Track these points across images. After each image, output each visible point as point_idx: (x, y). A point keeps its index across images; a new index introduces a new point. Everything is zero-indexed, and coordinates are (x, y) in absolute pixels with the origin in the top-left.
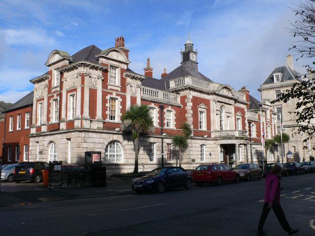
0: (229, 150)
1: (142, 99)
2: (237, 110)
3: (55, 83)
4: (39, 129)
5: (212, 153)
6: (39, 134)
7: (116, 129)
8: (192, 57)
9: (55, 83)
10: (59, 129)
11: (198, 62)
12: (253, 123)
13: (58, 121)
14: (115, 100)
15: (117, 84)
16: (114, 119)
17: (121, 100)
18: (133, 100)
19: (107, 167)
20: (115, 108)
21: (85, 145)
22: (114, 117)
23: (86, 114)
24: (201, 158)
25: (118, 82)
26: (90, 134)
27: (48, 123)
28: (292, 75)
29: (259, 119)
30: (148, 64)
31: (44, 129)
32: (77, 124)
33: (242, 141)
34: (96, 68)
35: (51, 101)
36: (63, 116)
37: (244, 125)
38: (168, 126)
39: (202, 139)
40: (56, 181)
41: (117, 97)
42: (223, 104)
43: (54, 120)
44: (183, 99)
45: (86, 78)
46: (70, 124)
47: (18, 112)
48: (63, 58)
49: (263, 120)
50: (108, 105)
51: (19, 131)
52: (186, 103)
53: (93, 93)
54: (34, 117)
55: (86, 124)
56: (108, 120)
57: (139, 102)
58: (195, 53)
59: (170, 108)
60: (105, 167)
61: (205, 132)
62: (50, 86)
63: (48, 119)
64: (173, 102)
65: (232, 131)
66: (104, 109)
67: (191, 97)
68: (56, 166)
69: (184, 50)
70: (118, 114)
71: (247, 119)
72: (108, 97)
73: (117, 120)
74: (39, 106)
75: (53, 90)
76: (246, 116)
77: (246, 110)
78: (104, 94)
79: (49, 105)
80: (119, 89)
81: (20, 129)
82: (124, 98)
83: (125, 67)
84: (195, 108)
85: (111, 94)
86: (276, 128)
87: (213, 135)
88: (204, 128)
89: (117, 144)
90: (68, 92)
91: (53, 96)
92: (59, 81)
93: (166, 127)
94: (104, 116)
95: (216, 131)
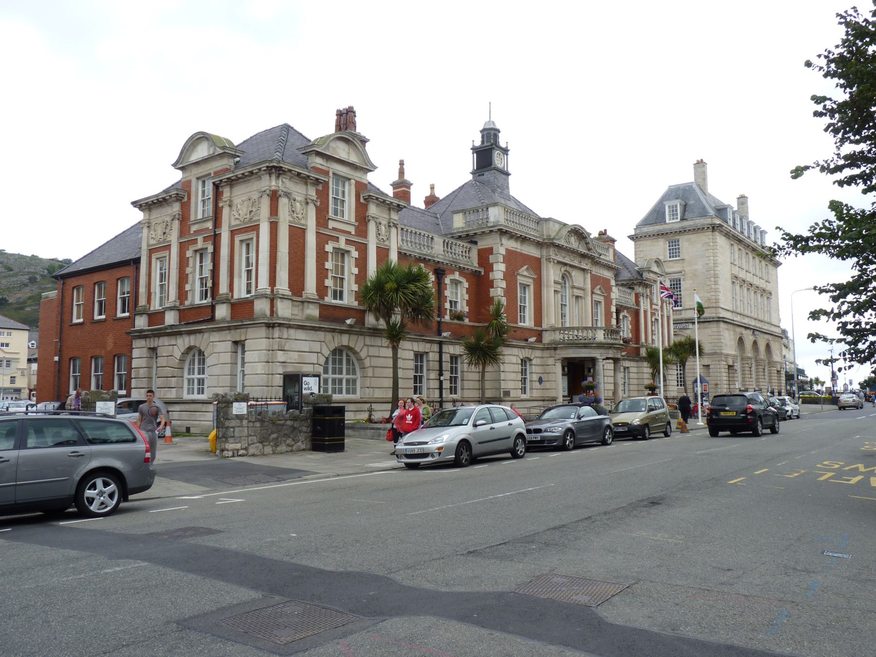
0: (578, 375)
1: (399, 253)
2: (596, 281)
3: (200, 209)
4: (156, 317)
5: (544, 377)
6: (158, 329)
7: (348, 322)
8: (498, 160)
9: (200, 209)
10: (212, 319)
11: (510, 171)
12: (625, 313)
13: (209, 299)
14: (456, 284)
15: (346, 218)
16: (341, 298)
17: (355, 254)
18: (383, 253)
19: (348, 407)
20: (343, 274)
21: (281, 356)
22: (341, 292)
23: (283, 285)
24: (415, 387)
25: (349, 212)
26: (292, 332)
27: (182, 303)
28: (707, 206)
29: (637, 303)
30: (402, 172)
31: (171, 318)
32: (261, 307)
33: (611, 351)
34: (304, 178)
35: (189, 254)
36: (223, 288)
37: (608, 314)
39: (523, 347)
40: (238, 439)
41: (348, 248)
42: (568, 268)
43: (196, 298)
44: (485, 256)
45: (283, 202)
46: (242, 310)
47: (97, 277)
48: (221, 151)
49: (644, 305)
50: (329, 265)
51: (100, 321)
52: (492, 264)
53: (297, 235)
54: (142, 290)
55: (284, 310)
56: (329, 300)
57: (394, 257)
58: (505, 151)
59: (457, 276)
60: (344, 407)
61: (530, 330)
62: (184, 219)
63: (182, 294)
64: (463, 262)
65: (586, 328)
66: (322, 273)
67: (503, 251)
68: (235, 404)
69: (478, 143)
70: (350, 287)
71: (614, 303)
72: (329, 248)
73: (349, 300)
74: (156, 266)
75: (194, 228)
76: (613, 296)
77: (613, 283)
78: (322, 240)
79: (183, 262)
80: (352, 230)
81: (81, 320)
82: (363, 249)
84: (510, 276)
86: (672, 322)
87: (547, 338)
88: (529, 322)
89: (347, 355)
90: (233, 233)
91: (195, 241)
92: (210, 207)
94: (322, 290)
95: (554, 330)
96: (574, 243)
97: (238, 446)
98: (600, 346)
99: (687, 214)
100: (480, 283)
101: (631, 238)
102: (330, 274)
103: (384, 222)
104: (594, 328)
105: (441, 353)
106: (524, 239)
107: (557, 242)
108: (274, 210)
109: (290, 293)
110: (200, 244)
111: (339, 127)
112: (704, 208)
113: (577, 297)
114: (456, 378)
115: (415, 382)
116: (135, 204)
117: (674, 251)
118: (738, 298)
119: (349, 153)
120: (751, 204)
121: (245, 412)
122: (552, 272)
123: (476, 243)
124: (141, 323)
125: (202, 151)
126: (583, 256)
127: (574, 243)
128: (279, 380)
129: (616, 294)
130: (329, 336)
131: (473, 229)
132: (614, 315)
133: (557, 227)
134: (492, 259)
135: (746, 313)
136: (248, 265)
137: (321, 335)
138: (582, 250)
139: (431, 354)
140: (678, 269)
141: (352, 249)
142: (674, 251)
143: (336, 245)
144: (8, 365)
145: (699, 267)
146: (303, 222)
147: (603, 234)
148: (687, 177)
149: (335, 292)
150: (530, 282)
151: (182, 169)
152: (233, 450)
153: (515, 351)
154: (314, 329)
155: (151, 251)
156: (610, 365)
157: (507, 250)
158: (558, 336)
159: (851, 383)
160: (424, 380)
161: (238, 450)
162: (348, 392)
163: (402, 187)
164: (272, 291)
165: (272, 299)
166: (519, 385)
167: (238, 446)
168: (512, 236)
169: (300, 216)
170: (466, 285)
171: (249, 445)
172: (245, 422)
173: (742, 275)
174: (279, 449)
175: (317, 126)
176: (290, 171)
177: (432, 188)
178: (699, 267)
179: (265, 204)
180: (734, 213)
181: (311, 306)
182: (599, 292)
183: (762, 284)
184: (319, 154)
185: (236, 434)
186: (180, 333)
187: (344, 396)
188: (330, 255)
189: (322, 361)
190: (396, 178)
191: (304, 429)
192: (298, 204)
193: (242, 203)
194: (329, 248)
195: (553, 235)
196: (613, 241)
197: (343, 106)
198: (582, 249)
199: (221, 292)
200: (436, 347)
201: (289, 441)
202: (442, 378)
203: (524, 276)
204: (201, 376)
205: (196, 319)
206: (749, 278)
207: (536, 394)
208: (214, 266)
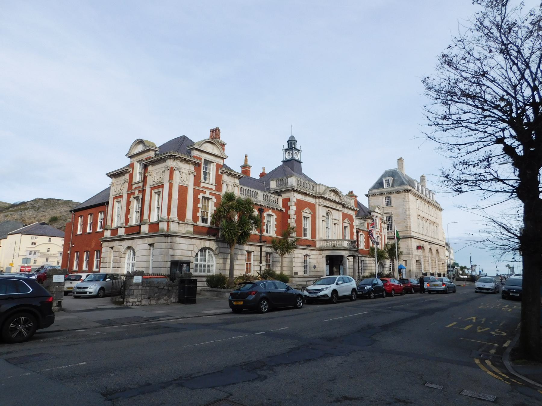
2: (345, 216)
3: (137, 177)
4: (114, 231)
6: (116, 238)
9: (137, 177)
10: (139, 233)
12: (361, 233)
15: (211, 182)
16: (206, 223)
19: (199, 279)
20: (208, 210)
23: (174, 215)
27: (126, 224)
30: (246, 161)
31: (121, 232)
32: (163, 226)
36: (145, 217)
37: (352, 234)
38: (267, 232)
40: (136, 296)
41: (210, 197)
42: (330, 209)
43: (134, 221)
44: (286, 202)
45: (176, 173)
50: (200, 205)
53: (183, 190)
54: (109, 217)
55: (174, 227)
56: (199, 223)
59: (270, 212)
63: (127, 220)
66: (196, 210)
71: (355, 227)
72: (200, 196)
75: (134, 186)
76: (354, 224)
77: (354, 217)
78: (196, 193)
79: (129, 203)
80: (213, 188)
83: (221, 162)
84: (298, 213)
85: (205, 192)
86: (386, 238)
87: (318, 245)
88: (309, 236)
89: (209, 252)
90: (152, 188)
91: (134, 193)
93: (265, 234)
94: (195, 218)
96: (333, 196)
97: (136, 300)
98: (345, 249)
99: (393, 184)
100: (283, 216)
101: (366, 195)
102: (200, 210)
103: (231, 184)
104: (343, 240)
105: (261, 251)
106: (306, 194)
107: (323, 196)
108: (171, 177)
109: (178, 219)
110: (136, 195)
111: (212, 137)
112: (403, 181)
113: (335, 224)
114: (269, 265)
115: (247, 266)
116: (108, 175)
117: (389, 203)
118: (428, 229)
119: (213, 149)
120: (405, 163)
121: (140, 281)
122: (321, 211)
123: (281, 196)
124: (108, 234)
125: (140, 148)
126: (338, 203)
127: (333, 196)
128: (169, 264)
129: (356, 222)
130: (198, 241)
131: (281, 188)
132: (355, 234)
133: (324, 188)
134: (289, 204)
135: (425, 234)
136: (158, 205)
137: (194, 241)
138: (337, 200)
139: (255, 252)
140: (390, 211)
141: (213, 197)
142: (389, 203)
143: (205, 196)
144: (35, 254)
145: (400, 210)
146: (186, 183)
147: (351, 193)
148: (393, 166)
149: (203, 219)
150: (309, 216)
151: (131, 157)
152: (132, 302)
153: (301, 251)
154: (190, 238)
155: (115, 198)
156: (351, 259)
157: (297, 200)
158: (325, 244)
159: (483, 271)
160: (252, 265)
161: (135, 302)
162: (200, 271)
163: (246, 168)
164: (168, 218)
165: (169, 221)
166: (303, 269)
167: (136, 300)
168: (300, 192)
169: (185, 180)
170: (276, 217)
171: (142, 299)
172: (140, 287)
173: (423, 215)
174: (160, 302)
175: (198, 135)
176: (180, 157)
177: (264, 169)
178: (400, 210)
179: (168, 173)
180: (418, 183)
181: (189, 226)
182: (347, 222)
183: (433, 219)
184: (197, 149)
185: (135, 293)
186: (124, 240)
187: (198, 273)
188: (201, 201)
189: (194, 254)
190: (243, 163)
191: (175, 291)
192: (184, 174)
193: (156, 173)
194: (200, 196)
195: (322, 192)
196: (356, 197)
197: (214, 127)
198: (336, 200)
199: (144, 218)
200: (258, 249)
201: (166, 298)
202: (261, 265)
203: (306, 212)
204: (133, 262)
205: (133, 232)
206: (426, 216)
207: (312, 274)
208: (142, 206)
